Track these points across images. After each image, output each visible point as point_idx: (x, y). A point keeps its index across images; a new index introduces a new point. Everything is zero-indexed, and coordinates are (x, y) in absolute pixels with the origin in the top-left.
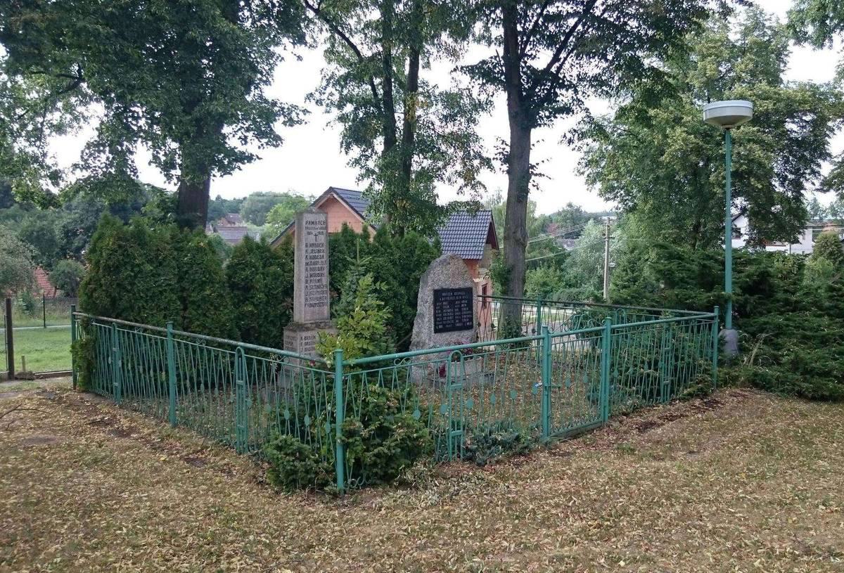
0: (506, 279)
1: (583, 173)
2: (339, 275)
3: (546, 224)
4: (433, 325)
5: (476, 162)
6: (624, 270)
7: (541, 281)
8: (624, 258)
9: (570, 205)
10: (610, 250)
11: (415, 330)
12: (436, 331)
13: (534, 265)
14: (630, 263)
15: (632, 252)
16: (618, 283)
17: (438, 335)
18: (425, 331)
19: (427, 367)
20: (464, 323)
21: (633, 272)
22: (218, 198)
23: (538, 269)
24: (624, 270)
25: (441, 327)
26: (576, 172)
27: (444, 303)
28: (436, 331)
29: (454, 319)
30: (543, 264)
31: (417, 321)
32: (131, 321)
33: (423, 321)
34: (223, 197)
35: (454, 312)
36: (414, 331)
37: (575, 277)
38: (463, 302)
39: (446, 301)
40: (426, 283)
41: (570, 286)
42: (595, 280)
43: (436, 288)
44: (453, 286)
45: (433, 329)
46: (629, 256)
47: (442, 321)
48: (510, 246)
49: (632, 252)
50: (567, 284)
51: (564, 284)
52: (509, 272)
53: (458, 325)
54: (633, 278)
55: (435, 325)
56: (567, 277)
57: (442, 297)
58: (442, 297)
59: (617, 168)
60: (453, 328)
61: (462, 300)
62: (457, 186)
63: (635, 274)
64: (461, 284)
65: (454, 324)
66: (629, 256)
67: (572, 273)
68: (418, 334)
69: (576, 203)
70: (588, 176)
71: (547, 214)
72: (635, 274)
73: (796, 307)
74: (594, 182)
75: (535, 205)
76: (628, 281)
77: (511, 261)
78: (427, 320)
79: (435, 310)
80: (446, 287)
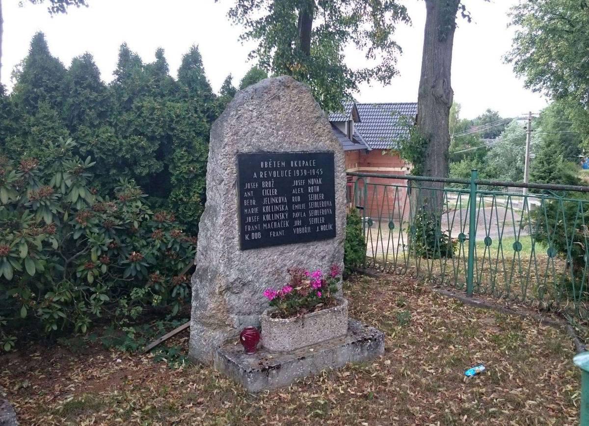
0: (421, 154)
1: (510, 61)
2: (89, 131)
3: (467, 125)
4: (236, 233)
5: (388, 15)
6: (540, 163)
7: (465, 172)
8: (541, 152)
9: (489, 111)
10: (531, 144)
11: (201, 242)
12: (246, 245)
13: (459, 158)
14: (546, 156)
15: (548, 146)
16: (535, 173)
17: (246, 254)
18: (218, 245)
19: (222, 325)
20: (314, 226)
21: (549, 163)
22: (94, 62)
23: (462, 161)
24: (540, 163)
25: (257, 236)
26: (503, 59)
27: (265, 184)
28: (246, 245)
29: (292, 220)
30: (467, 157)
31: (205, 223)
32: (349, 196)
33: (213, 225)
34: (95, 64)
35: (290, 203)
36: (199, 247)
37: (495, 169)
38: (312, 181)
39: (268, 179)
40: (220, 138)
41: (490, 176)
42: (513, 172)
43: (245, 150)
44: (286, 148)
45: (236, 241)
46: (546, 149)
47: (261, 222)
48: (426, 106)
49: (548, 146)
50: (487, 175)
51: (484, 175)
52: (425, 144)
53: (299, 231)
54: (549, 169)
55: (243, 232)
56: (487, 169)
57: (259, 169)
58: (259, 169)
59: (549, 52)
60: (289, 238)
61: (309, 177)
62: (366, 49)
63: (551, 166)
64: (306, 143)
65: (288, 230)
66: (546, 149)
67: (492, 164)
68: (206, 249)
69: (494, 109)
70: (516, 63)
71: (469, 119)
72: (551, 166)
73: (457, 191)
74: (523, 69)
75: (459, 106)
76: (544, 172)
77: (428, 129)
78: (220, 221)
79: (242, 198)
80: (272, 149)
